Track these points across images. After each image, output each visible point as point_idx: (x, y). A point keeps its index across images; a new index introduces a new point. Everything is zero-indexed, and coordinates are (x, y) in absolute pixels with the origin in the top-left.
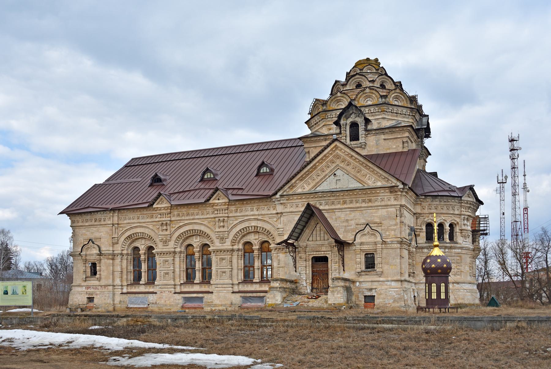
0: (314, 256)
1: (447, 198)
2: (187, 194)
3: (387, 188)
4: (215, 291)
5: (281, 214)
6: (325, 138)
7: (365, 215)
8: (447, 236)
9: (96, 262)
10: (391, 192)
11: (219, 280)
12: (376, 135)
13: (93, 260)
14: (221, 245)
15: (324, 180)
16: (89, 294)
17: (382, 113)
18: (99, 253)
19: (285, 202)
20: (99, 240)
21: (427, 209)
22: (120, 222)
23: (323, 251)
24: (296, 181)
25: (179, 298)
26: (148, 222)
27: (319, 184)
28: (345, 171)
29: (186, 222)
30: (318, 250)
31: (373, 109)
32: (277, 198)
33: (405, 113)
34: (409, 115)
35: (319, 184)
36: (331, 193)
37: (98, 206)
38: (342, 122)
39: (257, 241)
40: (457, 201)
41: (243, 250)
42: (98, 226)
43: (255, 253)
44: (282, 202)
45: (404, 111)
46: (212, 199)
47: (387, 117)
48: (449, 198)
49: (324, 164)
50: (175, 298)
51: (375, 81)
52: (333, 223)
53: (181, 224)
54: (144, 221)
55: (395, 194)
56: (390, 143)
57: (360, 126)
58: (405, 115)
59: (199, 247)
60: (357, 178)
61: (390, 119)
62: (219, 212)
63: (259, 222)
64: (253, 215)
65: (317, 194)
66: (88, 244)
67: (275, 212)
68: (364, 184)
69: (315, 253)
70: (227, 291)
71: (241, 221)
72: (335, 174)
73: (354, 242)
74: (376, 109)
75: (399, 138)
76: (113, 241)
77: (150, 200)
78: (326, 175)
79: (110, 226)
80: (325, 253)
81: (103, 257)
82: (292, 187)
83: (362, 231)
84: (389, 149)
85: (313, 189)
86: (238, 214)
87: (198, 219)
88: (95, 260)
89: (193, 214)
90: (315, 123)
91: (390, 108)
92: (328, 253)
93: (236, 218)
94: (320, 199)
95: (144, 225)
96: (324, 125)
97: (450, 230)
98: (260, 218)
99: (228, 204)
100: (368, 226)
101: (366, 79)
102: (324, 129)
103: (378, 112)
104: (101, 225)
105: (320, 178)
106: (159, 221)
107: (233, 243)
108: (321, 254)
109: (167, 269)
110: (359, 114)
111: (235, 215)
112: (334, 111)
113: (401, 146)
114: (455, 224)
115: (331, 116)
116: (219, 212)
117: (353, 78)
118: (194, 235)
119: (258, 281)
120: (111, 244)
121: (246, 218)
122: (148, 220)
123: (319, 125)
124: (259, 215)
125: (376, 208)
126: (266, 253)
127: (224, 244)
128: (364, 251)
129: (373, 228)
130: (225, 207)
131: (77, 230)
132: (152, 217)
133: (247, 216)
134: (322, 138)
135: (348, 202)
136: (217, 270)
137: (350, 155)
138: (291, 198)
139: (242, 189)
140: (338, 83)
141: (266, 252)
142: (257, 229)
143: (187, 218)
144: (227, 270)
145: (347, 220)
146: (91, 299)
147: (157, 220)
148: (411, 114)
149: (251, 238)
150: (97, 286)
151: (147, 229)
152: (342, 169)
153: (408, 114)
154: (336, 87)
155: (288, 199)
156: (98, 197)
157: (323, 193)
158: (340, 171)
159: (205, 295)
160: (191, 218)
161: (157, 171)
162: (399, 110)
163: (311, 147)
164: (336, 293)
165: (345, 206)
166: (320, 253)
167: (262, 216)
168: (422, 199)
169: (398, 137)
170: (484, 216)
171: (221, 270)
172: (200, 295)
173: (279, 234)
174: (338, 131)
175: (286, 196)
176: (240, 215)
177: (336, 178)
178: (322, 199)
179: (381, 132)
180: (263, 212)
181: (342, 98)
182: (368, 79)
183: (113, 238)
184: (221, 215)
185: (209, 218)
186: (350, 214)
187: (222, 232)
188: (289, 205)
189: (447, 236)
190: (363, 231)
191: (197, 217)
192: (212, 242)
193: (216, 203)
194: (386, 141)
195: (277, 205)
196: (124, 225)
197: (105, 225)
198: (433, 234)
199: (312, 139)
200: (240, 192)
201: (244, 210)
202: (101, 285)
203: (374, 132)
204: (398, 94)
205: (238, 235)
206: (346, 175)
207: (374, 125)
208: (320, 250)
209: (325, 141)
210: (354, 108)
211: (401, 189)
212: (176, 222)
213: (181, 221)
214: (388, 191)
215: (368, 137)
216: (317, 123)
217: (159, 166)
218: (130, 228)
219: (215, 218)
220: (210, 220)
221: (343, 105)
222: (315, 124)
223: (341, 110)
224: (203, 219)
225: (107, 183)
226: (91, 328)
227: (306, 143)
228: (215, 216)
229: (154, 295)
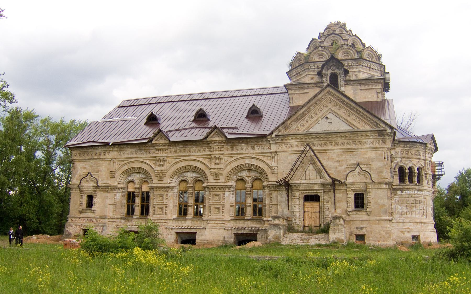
0: (307, 194)
1: (416, 144)
2: (148, 135)
3: (376, 132)
4: (208, 227)
5: (275, 154)
6: (308, 86)
7: (355, 156)
8: (415, 180)
9: (93, 195)
10: (379, 136)
11: (211, 216)
12: (353, 85)
13: (90, 193)
14: (215, 181)
15: (316, 122)
17: (358, 66)
18: (97, 186)
19: (279, 141)
20: (97, 173)
21: (399, 154)
23: (315, 190)
24: (291, 122)
26: (145, 157)
27: (312, 125)
28: (336, 115)
29: (183, 158)
30: (310, 189)
31: (351, 63)
32: (272, 138)
33: (375, 68)
34: (379, 70)
35: (312, 125)
36: (324, 134)
37: (99, 141)
38: (324, 72)
39: (250, 178)
40: (423, 147)
41: (235, 187)
43: (248, 190)
44: (277, 141)
45: (375, 66)
46: (209, 137)
47: (362, 70)
48: (417, 144)
49: (317, 107)
51: (348, 40)
52: (325, 163)
53: (177, 160)
55: (383, 137)
56: (366, 93)
57: (339, 77)
58: (376, 70)
59: (192, 183)
60: (348, 121)
61: (365, 72)
63: (253, 160)
64: (247, 154)
65: (311, 135)
66: (87, 176)
67: (269, 151)
69: (308, 192)
70: (220, 227)
71: (236, 159)
72: (327, 117)
73: (346, 182)
74: (354, 62)
75: (374, 89)
77: (148, 136)
78: (319, 118)
79: (108, 160)
80: (318, 191)
81: (100, 190)
83: (353, 172)
84: (365, 98)
85: (306, 131)
86: (234, 152)
88: (92, 193)
90: (297, 73)
91: (365, 63)
92: (320, 191)
93: (231, 156)
95: (142, 160)
96: (307, 75)
97: (409, 173)
98: (254, 156)
99: (168, 144)
100: (358, 167)
101: (340, 38)
102: (306, 78)
105: (313, 120)
106: (156, 157)
107: (228, 178)
108: (313, 193)
109: (160, 204)
110: (339, 66)
111: (231, 153)
112: (316, 63)
113: (375, 95)
114: (421, 169)
115: (314, 67)
116: (159, 152)
117: (330, 37)
118: (189, 171)
119: (249, 218)
121: (241, 156)
123: (301, 75)
124: (253, 153)
125: (365, 150)
126: (257, 191)
127: (219, 181)
128: (86, 193)
129: (363, 169)
130: (165, 147)
131: (160, 133)
133: (242, 154)
134: (305, 86)
135: (340, 143)
136: (210, 206)
137: (341, 100)
138: (286, 138)
139: (237, 128)
140: (315, 41)
141: (258, 190)
142: (251, 167)
143: (184, 155)
144: (220, 206)
145: (338, 160)
148: (380, 70)
149: (244, 174)
150: (92, 218)
151: (144, 164)
152: (333, 112)
153: (378, 69)
154: (313, 44)
155: (283, 138)
156: (89, 133)
157: (316, 134)
158: (332, 114)
160: (188, 155)
161: (153, 111)
162: (372, 65)
163: (295, 94)
164: (337, 231)
165: (337, 147)
166: (313, 192)
168: (396, 144)
169: (373, 88)
170: (439, 163)
171: (214, 206)
173: (272, 172)
174: (319, 81)
175: (281, 136)
176: (236, 153)
177: (328, 121)
178: (315, 140)
179: (358, 83)
181: (323, 52)
182: (342, 38)
184: (161, 155)
186: (341, 155)
187: (217, 169)
188: (283, 144)
189: (415, 180)
190: (354, 171)
192: (206, 178)
193: (213, 141)
194: (362, 91)
195: (272, 145)
197: (105, 159)
198: (404, 176)
199: (296, 87)
200: (235, 131)
202: (95, 217)
203: (352, 83)
204: (370, 52)
205: (132, 170)
206: (336, 118)
207: (352, 77)
208: (313, 189)
209: (308, 88)
210: (334, 61)
211: (389, 132)
212: (172, 158)
213: (177, 158)
214: (377, 134)
215: (346, 87)
216: (300, 73)
218: (128, 162)
219: (210, 155)
220: (206, 156)
221: (323, 58)
222: (297, 74)
223: (324, 62)
225: (104, 120)
227: (290, 90)
228: (211, 153)
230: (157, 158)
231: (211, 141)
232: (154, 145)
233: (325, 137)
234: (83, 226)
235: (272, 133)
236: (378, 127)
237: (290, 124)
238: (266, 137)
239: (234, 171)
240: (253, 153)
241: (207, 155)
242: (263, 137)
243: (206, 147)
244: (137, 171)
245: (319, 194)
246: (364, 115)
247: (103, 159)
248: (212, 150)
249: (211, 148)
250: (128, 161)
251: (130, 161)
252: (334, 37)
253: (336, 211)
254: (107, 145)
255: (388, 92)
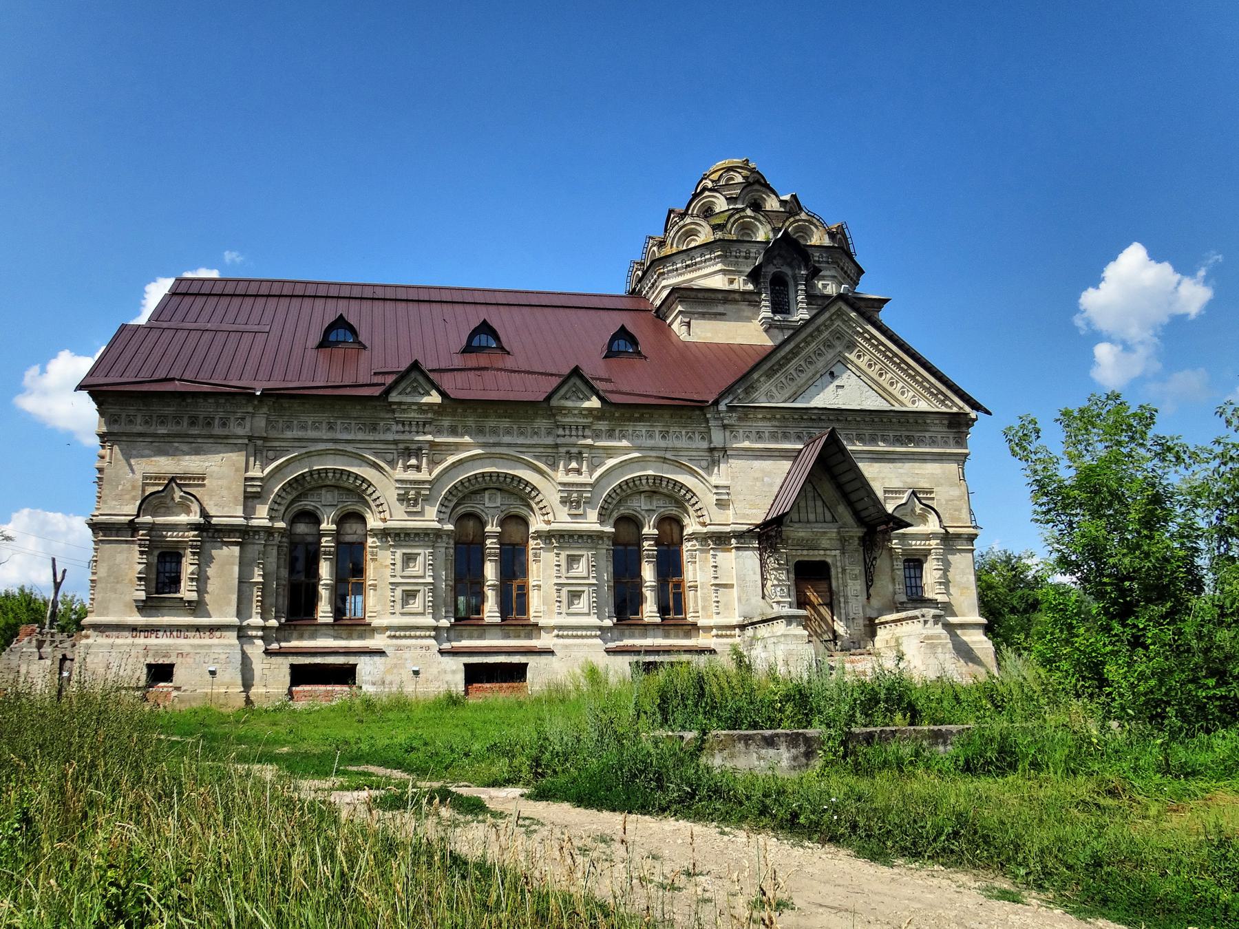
0: (801, 559)
10: (950, 426)
15: (811, 382)
16: (156, 654)
22: (273, 434)
25: (454, 668)
26: (361, 441)
27: (803, 389)
42: (199, 440)
50: (442, 666)
54: (349, 438)
62: (567, 432)
68: (892, 401)
76: (249, 489)
79: (240, 441)
81: (210, 534)
82: (750, 389)
87: (509, 445)
89: (494, 431)
92: (833, 553)
94: (810, 424)
95: (349, 448)
103: (828, 262)
104: (211, 436)
106: (396, 442)
108: (816, 556)
120: (241, 498)
122: (360, 436)
129: (923, 501)
131: (413, 375)
132: (374, 428)
146: (161, 673)
147: (390, 437)
149: (639, 505)
159: (532, 661)
160: (491, 441)
167: (674, 453)
172: (351, 660)
180: (678, 444)
183: (246, 479)
185: (539, 446)
188: (741, 431)
191: (507, 439)
196: (282, 444)
197: (227, 437)
201: (630, 432)
217: (137, 362)
219: (557, 446)
220: (542, 450)
224: (522, 445)
226: (1169, 604)
229: (377, 659)
230: (401, 446)
231: (561, 409)
232: (395, 407)
233: (838, 420)
234: (150, 654)
235: (716, 403)
236: (946, 406)
237: (758, 380)
238: (701, 409)
239: (647, 482)
240: (666, 449)
241: (546, 446)
242: (693, 408)
243: (542, 424)
244: (333, 482)
245: (829, 560)
246: (918, 373)
247: (218, 437)
248: (560, 432)
249: (558, 427)
250: (303, 451)
251: (312, 449)
252: (706, 197)
253: (869, 602)
254: (246, 395)
255: (1098, 288)
